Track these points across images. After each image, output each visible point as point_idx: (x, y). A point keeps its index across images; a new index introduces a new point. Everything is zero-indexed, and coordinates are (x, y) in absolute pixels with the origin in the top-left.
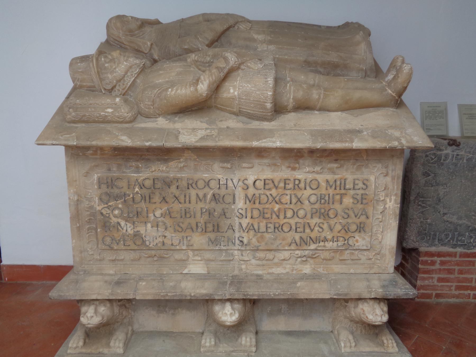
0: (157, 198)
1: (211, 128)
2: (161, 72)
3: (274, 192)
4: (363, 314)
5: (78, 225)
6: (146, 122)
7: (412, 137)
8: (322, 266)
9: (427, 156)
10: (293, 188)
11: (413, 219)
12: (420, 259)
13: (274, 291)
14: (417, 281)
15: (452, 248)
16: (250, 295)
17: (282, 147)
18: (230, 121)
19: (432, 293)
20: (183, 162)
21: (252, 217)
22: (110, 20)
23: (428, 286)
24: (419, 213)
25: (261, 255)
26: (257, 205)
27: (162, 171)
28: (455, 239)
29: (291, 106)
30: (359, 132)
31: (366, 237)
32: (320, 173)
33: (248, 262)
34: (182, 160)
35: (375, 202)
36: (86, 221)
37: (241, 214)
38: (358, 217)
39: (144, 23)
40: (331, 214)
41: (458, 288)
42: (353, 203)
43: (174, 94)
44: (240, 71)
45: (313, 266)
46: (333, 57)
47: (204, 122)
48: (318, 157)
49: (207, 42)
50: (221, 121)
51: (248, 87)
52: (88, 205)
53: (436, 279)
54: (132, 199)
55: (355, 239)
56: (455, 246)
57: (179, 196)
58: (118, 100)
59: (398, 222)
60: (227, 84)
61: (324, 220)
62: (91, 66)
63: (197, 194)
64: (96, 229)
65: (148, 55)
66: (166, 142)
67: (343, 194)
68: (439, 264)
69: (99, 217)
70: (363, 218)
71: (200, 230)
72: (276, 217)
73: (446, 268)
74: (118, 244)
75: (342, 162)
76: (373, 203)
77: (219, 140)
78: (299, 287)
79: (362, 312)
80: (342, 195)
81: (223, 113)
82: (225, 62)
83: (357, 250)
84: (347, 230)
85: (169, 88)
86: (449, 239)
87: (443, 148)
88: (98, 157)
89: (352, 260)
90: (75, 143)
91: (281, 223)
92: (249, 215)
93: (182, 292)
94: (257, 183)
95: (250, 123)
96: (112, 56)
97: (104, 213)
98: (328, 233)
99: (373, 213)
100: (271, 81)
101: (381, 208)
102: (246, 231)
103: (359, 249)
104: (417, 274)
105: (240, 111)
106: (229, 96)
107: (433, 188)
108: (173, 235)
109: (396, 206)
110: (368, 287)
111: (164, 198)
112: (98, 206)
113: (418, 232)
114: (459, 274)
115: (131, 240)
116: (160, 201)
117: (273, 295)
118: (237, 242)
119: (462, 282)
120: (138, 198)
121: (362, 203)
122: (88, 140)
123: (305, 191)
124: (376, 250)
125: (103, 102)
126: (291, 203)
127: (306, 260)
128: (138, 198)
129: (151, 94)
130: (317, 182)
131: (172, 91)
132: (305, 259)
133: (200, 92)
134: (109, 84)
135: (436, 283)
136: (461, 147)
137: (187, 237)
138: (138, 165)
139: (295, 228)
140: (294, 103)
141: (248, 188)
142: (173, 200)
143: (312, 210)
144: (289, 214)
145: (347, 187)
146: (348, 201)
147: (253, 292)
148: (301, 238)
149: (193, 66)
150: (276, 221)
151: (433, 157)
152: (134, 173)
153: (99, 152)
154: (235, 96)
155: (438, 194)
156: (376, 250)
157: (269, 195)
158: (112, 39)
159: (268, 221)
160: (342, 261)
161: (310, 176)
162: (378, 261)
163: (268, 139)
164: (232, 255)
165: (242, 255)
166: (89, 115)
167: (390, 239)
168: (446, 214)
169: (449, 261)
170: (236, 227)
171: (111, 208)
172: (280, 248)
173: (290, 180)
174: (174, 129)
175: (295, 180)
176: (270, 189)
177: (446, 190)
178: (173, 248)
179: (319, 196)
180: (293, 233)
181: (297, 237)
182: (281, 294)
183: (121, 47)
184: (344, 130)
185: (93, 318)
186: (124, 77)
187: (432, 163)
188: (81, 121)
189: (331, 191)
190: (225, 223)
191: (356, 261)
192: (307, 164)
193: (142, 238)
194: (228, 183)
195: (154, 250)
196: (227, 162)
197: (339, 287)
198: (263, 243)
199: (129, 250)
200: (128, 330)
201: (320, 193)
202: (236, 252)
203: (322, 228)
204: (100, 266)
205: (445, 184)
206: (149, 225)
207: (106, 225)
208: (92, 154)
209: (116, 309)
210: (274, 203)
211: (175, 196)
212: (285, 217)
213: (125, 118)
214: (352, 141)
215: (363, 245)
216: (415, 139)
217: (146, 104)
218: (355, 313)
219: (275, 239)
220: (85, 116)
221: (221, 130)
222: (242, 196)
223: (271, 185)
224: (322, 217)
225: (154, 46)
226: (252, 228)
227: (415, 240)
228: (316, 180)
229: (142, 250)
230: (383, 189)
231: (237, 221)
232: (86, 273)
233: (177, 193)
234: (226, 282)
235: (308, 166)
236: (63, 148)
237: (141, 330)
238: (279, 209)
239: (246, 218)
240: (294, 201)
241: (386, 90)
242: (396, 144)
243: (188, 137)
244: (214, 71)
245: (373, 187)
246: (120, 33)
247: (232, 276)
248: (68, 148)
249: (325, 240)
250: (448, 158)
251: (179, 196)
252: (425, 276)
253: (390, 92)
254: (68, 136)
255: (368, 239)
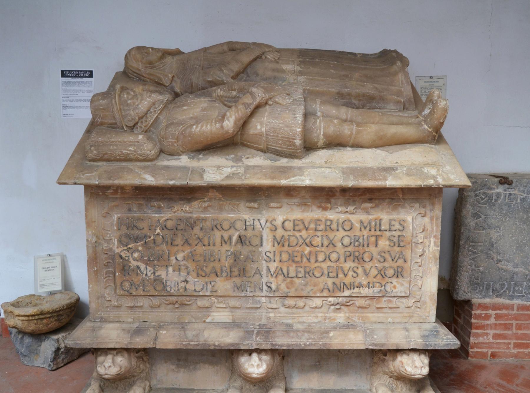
0: (179, 241)
1: (237, 166)
2: (185, 108)
3: (304, 233)
4: (402, 367)
5: (96, 269)
6: (169, 160)
7: (449, 175)
8: (357, 315)
9: (476, 195)
10: (324, 229)
11: (464, 266)
12: (473, 312)
13: (303, 341)
14: (470, 338)
15: (509, 299)
16: (279, 345)
17: (311, 185)
18: (258, 158)
19: (487, 352)
20: (207, 201)
21: (281, 261)
22: (129, 52)
23: (483, 343)
24: (470, 259)
25: (291, 302)
26: (286, 248)
27: (185, 212)
28: (512, 289)
29: (321, 143)
30: (394, 170)
31: (404, 283)
32: (353, 213)
33: (277, 310)
34: (206, 199)
35: (413, 244)
36: (104, 265)
37: (268, 257)
38: (395, 260)
39: (167, 53)
40: (366, 258)
41: (517, 346)
42: (390, 245)
43: (199, 131)
44: (267, 107)
45: (347, 315)
46: (369, 89)
47: (230, 160)
48: (351, 196)
49: (232, 75)
50: (248, 158)
51: (276, 123)
52: (106, 247)
53: (492, 335)
54: (152, 241)
55: (392, 285)
56: (512, 297)
57: (202, 238)
58: (140, 137)
59: (438, 267)
60: (254, 120)
61: (358, 264)
62: (114, 103)
63: (222, 236)
64: (114, 274)
65: (168, 87)
66: (190, 180)
67: (379, 236)
68: (495, 318)
69: (118, 260)
70: (400, 262)
71: (224, 274)
72: (307, 261)
73: (503, 322)
74: (137, 289)
75: (377, 201)
76: (412, 245)
77: (245, 179)
78: (332, 337)
79: (401, 365)
80: (377, 237)
81: (249, 150)
82: (252, 98)
83: (394, 297)
84: (383, 275)
85: (194, 125)
86: (504, 289)
87: (494, 186)
88: (118, 196)
89: (390, 308)
90: (97, 183)
91: (313, 267)
92: (277, 259)
93: (205, 341)
94: (286, 223)
95: (279, 161)
96: (134, 92)
97: (124, 256)
98: (363, 278)
99: (411, 257)
100: (300, 118)
101: (420, 251)
102: (275, 275)
103: (397, 296)
104: (469, 330)
105: (267, 147)
106: (256, 132)
107: (484, 231)
108: (196, 280)
109: (437, 248)
110: (407, 337)
111: (186, 240)
112: (117, 248)
113: (470, 282)
114: (517, 329)
115: (151, 285)
116: (182, 243)
117: (303, 346)
118: (265, 288)
119: (522, 339)
120: (159, 239)
121: (399, 246)
122: (110, 179)
123: (338, 232)
124: (416, 298)
125: (126, 140)
126: (322, 246)
127: (340, 308)
128: (159, 239)
129: (175, 131)
130: (350, 223)
131: (197, 127)
132: (339, 307)
133: (226, 129)
134: (131, 121)
135: (491, 340)
136: (513, 185)
137: (211, 283)
138: (160, 205)
139: (327, 273)
140: (325, 140)
141: (276, 229)
142: (196, 242)
143: (345, 254)
144: (321, 258)
145: (383, 228)
146: (383, 243)
147: (283, 341)
148: (334, 283)
149: (218, 101)
150: (306, 265)
151: (483, 197)
152: (156, 214)
153: (119, 191)
154: (262, 132)
155: (491, 238)
156: (416, 298)
157: (298, 237)
158: (130, 72)
159: (298, 265)
160: (380, 309)
161: (343, 217)
162: (419, 310)
163: (297, 177)
164: (259, 301)
165: (270, 302)
166: (111, 153)
167: (431, 285)
168: (500, 261)
169: (506, 315)
170: (264, 272)
171: (131, 251)
172: (311, 294)
173: (321, 220)
174: (198, 167)
175: (326, 220)
176: (300, 231)
177: (498, 234)
178: (196, 294)
179: (353, 238)
180: (325, 278)
181: (330, 282)
182: (312, 344)
183: (140, 79)
184: (378, 168)
185: (110, 369)
186: (147, 113)
187: (483, 204)
188: (101, 160)
189: (365, 233)
190: (252, 268)
191: (394, 309)
192: (339, 204)
193: (163, 283)
194: (255, 224)
195: (175, 296)
196: (254, 201)
197: (375, 337)
198: (293, 289)
199: (149, 296)
200: (145, 385)
201: (353, 235)
202: (263, 299)
203: (356, 273)
204: (117, 313)
205: (499, 227)
206: (170, 269)
207: (125, 269)
208: (112, 194)
209: (134, 361)
210: (304, 246)
211: (198, 238)
212: (316, 261)
213: (148, 155)
214: (385, 179)
215: (401, 292)
216: (452, 177)
217: (169, 142)
218: (394, 367)
219: (306, 285)
220: (106, 154)
221: (248, 168)
222: (271, 238)
223: (301, 227)
224: (356, 260)
225: (175, 79)
226: (280, 272)
227: (466, 291)
228: (350, 221)
229: (162, 296)
230: (421, 231)
231: (264, 264)
232: (103, 320)
233: (201, 234)
234: (253, 331)
235: (341, 205)
236: (82, 187)
237: (159, 386)
238: (310, 253)
239: (274, 261)
240: (326, 243)
241: (422, 125)
242: (431, 182)
243: (213, 176)
244: (241, 107)
245: (411, 228)
246: (139, 65)
247: (259, 325)
248: (88, 187)
249: (360, 286)
250: (500, 198)
251: (202, 238)
252: (479, 332)
253: (426, 127)
254: (90, 175)
255: (407, 285)
